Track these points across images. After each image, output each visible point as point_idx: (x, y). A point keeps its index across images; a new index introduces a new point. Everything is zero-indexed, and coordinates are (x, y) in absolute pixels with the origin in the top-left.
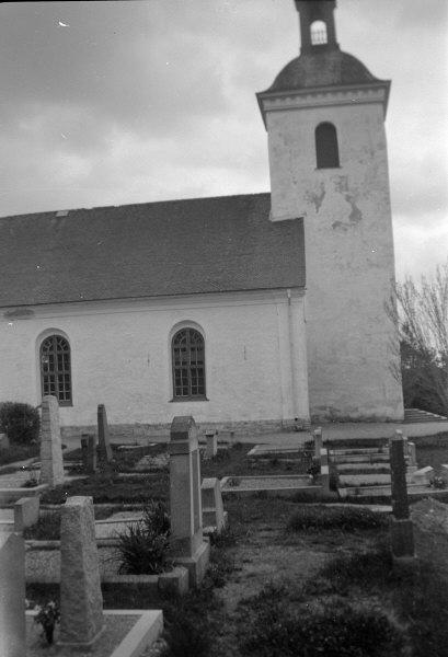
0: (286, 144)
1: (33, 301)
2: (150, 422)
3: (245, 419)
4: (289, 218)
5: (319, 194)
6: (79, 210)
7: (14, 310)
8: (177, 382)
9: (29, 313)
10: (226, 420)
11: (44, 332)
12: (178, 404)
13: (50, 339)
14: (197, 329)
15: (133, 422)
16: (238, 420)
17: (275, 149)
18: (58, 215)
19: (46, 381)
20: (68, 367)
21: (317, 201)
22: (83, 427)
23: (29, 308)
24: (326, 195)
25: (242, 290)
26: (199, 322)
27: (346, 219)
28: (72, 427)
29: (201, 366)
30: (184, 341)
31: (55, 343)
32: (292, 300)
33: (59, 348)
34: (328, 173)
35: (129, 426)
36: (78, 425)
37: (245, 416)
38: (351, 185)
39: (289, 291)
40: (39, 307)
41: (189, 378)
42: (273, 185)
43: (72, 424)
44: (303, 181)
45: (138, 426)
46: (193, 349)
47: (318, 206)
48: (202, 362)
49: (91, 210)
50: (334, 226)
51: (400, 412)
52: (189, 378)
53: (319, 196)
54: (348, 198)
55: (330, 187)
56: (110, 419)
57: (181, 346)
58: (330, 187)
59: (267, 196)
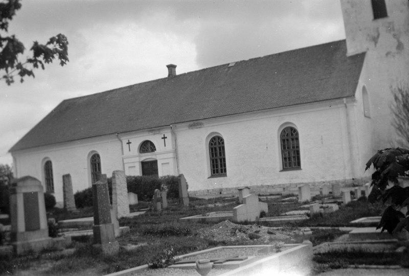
0: (352, 7)
1: (202, 117)
2: (269, 184)
3: (323, 180)
4: (357, 53)
5: (376, 35)
6: (241, 62)
7: (192, 123)
8: (284, 159)
9: (201, 124)
10: (312, 181)
11: (209, 136)
12: (216, 179)
13: (214, 138)
14: (217, 135)
15: (259, 184)
16: (320, 181)
17: (346, 12)
18: (230, 65)
19: (213, 162)
20: (224, 155)
21: (375, 40)
22: (232, 189)
23: (200, 121)
24: (380, 36)
25: (317, 101)
26: (293, 122)
27: (394, 50)
28: (226, 189)
29: (297, 149)
30: (215, 144)
31: (217, 141)
32: (347, 105)
33: (219, 143)
34: (380, 21)
35: (258, 187)
36: (230, 187)
37: (323, 178)
38: (396, 27)
39: (344, 99)
40: (206, 121)
41: (291, 155)
42: (347, 33)
43: (227, 187)
44: (365, 29)
45: (262, 187)
46: (292, 140)
47: (376, 43)
48: (298, 147)
49: (248, 61)
50: (387, 54)
51: (119, 217)
52: (291, 155)
53: (376, 37)
54: (394, 36)
55: (382, 30)
56: (68, 207)
57: (286, 137)
58: (382, 30)
59: (344, 41)
